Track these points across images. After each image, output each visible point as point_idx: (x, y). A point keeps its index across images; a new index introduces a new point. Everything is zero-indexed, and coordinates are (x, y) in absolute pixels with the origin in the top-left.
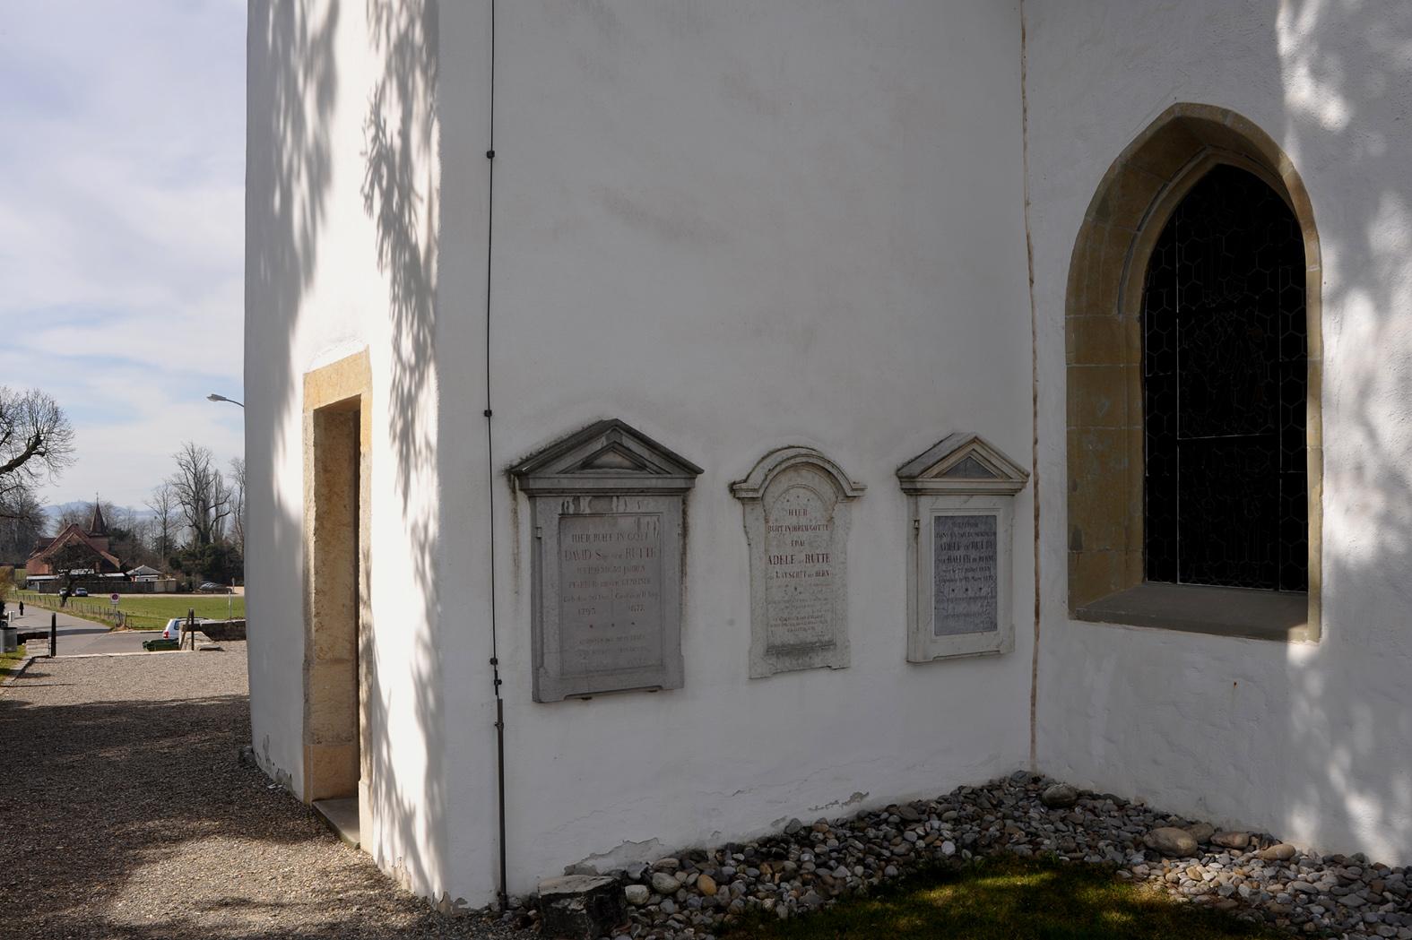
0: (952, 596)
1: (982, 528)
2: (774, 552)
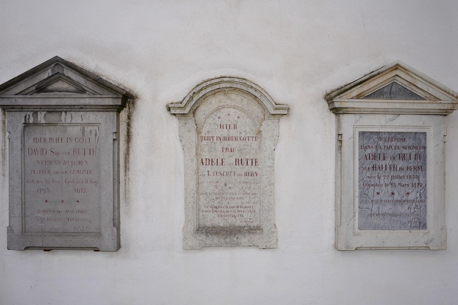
0: (377, 198)
1: (409, 142)
2: (206, 155)
